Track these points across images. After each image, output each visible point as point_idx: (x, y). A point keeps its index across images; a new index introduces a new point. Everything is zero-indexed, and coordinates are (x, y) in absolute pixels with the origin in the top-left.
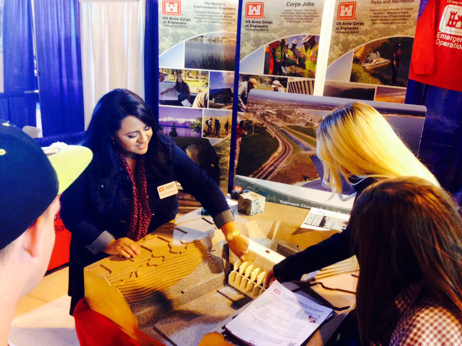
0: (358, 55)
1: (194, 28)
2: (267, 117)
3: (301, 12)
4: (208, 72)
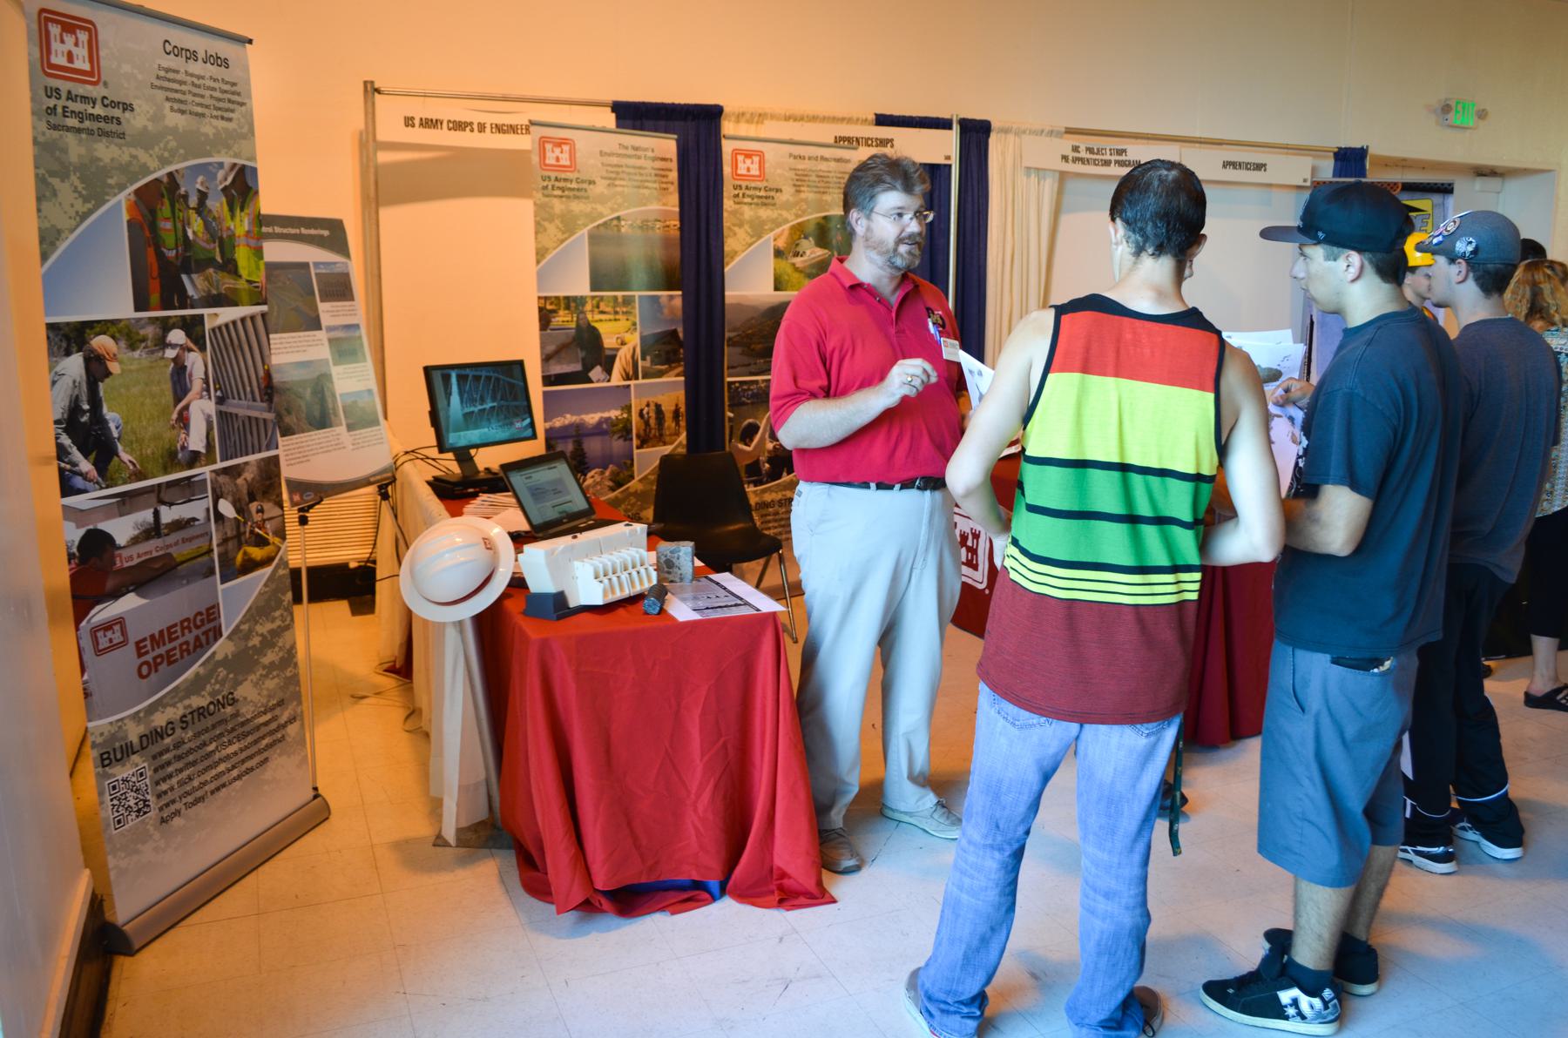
0: (781, 244)
1: (602, 199)
4: (634, 296)
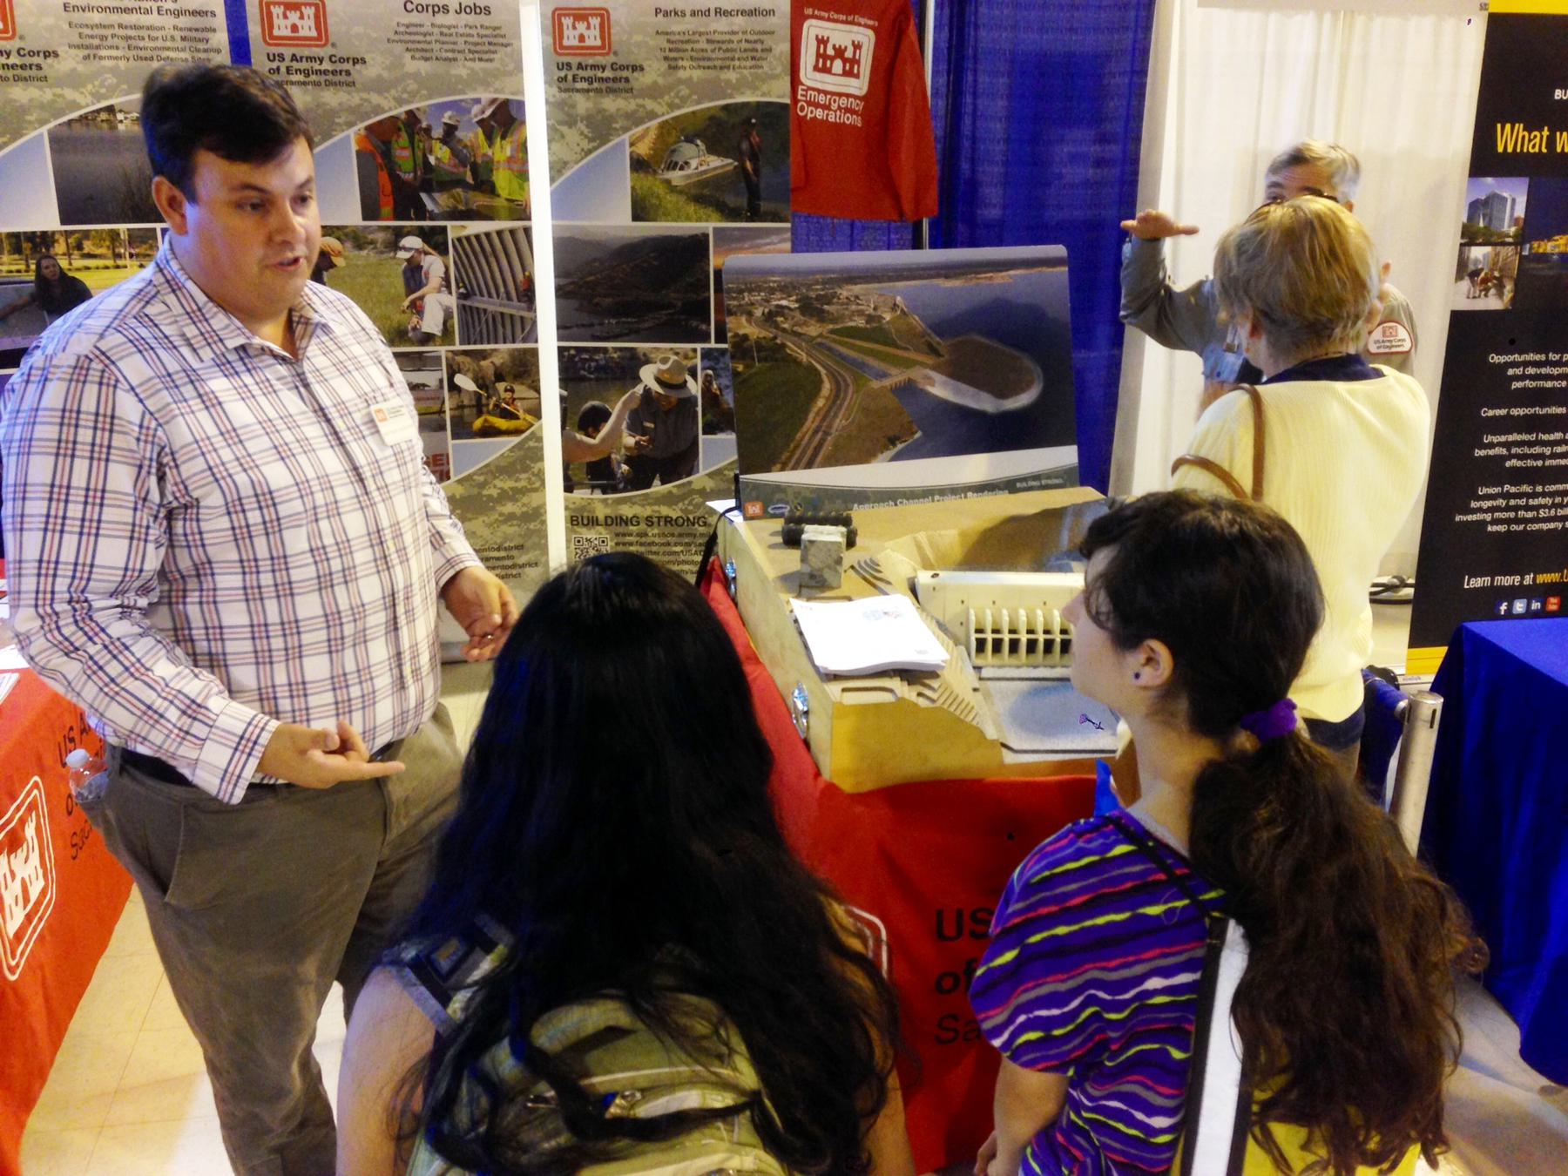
0: (643, 149)
1: (74, 80)
2: (780, 319)
3: (453, 30)
4: (155, 230)
